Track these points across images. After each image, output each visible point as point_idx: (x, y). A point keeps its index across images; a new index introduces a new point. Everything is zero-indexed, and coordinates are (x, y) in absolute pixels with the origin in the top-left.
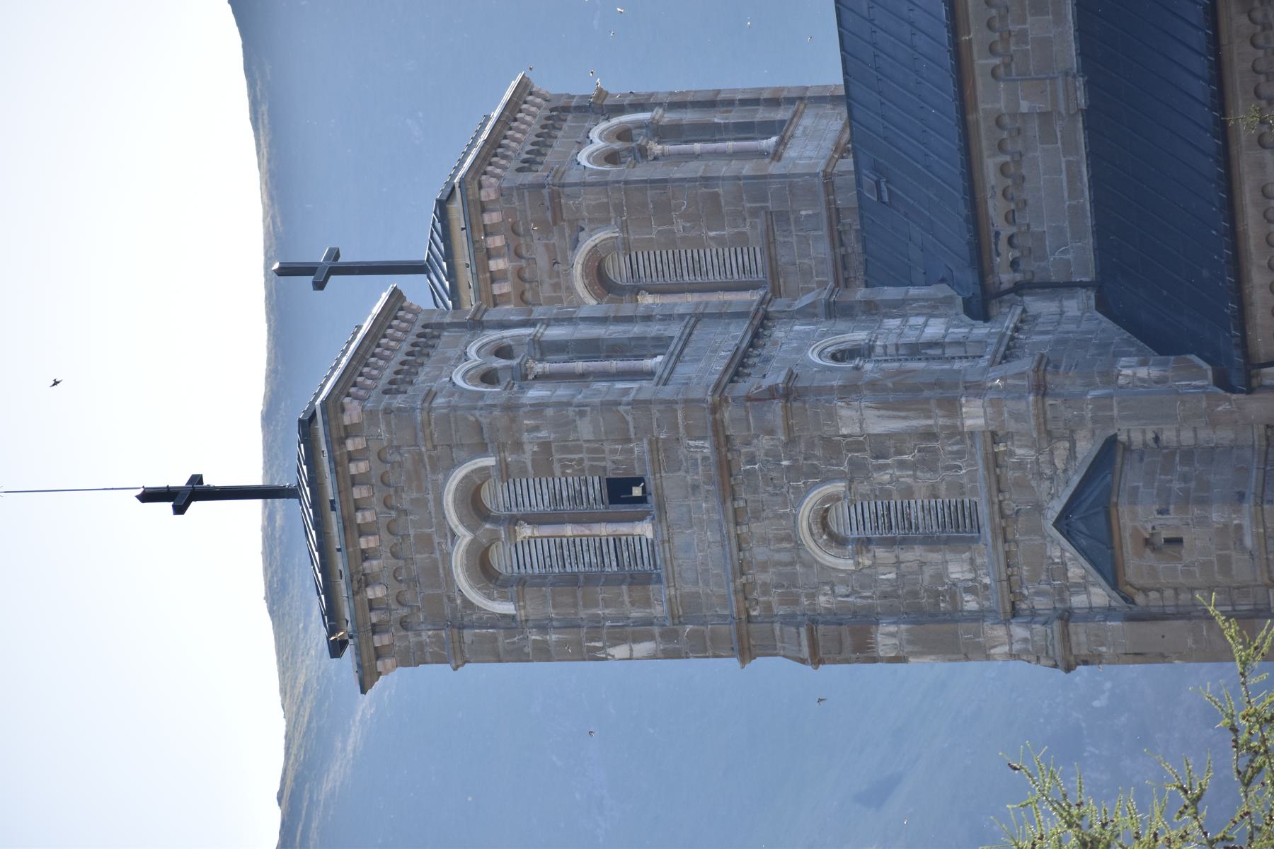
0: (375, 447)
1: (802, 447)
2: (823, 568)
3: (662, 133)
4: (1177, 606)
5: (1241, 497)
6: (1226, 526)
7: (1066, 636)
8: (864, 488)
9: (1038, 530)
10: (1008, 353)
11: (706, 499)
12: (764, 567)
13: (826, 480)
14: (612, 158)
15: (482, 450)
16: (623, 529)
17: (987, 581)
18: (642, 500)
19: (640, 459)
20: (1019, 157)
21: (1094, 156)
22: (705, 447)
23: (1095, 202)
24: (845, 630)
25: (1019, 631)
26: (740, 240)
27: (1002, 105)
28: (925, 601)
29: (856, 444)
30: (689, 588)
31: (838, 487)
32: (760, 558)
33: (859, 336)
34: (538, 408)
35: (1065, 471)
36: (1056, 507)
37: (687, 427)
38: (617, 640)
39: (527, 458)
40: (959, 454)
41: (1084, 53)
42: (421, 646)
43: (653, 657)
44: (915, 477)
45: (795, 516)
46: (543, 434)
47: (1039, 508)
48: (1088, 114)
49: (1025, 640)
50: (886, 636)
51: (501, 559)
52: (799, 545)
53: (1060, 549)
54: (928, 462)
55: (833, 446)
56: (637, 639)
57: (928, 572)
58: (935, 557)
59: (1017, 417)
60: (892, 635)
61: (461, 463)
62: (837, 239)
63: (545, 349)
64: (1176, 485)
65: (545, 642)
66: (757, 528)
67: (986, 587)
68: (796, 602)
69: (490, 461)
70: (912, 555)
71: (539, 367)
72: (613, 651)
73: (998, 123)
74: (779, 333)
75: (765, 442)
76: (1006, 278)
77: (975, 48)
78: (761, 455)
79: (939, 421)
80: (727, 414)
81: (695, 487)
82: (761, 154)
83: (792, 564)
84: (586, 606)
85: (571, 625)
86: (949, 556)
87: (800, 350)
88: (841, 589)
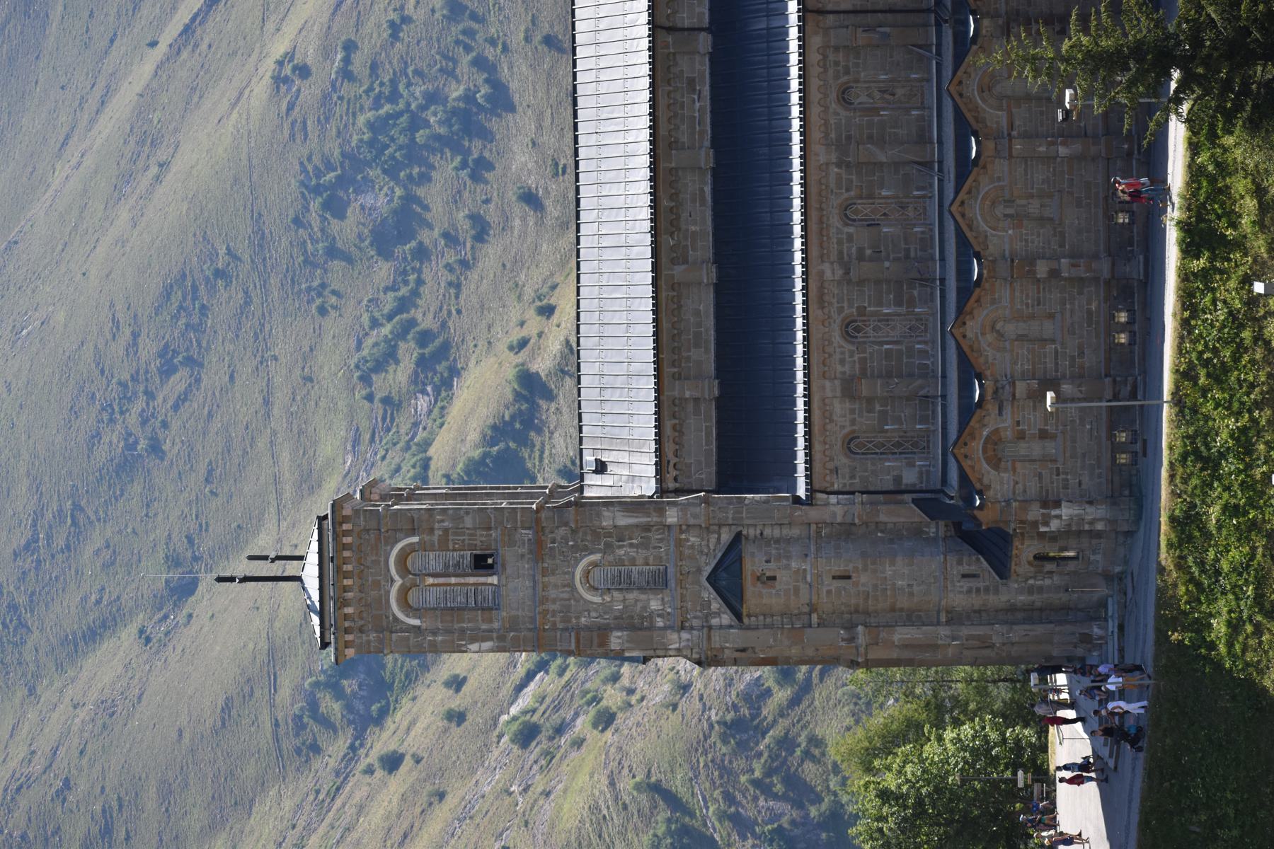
1: (581, 534)
2: (586, 601)
6: (799, 569)
7: (709, 638)
8: (611, 558)
11: (528, 563)
12: (554, 601)
15: (413, 532)
17: (669, 610)
18: (491, 567)
19: (496, 540)
21: (720, 422)
23: (719, 448)
24: (595, 634)
27: (676, 393)
30: (513, 613)
31: (596, 557)
32: (554, 596)
35: (714, 550)
37: (522, 522)
38: (473, 640)
39: (436, 538)
40: (661, 540)
42: (369, 642)
43: (492, 650)
44: (637, 552)
45: (574, 573)
46: (446, 524)
47: (699, 570)
48: (718, 400)
49: (688, 640)
50: (616, 640)
52: (574, 588)
53: (709, 593)
54: (645, 545)
56: (484, 640)
57: (639, 605)
58: (643, 597)
59: (695, 516)
60: (619, 637)
61: (400, 541)
64: (774, 552)
65: (435, 641)
66: (552, 579)
67: (669, 614)
68: (569, 621)
69: (415, 539)
70: (631, 596)
72: (470, 646)
77: (665, 363)
78: (558, 538)
79: (654, 519)
80: (543, 515)
81: (523, 556)
83: (569, 600)
84: (459, 622)
85: (448, 631)
86: (651, 597)
88: (594, 614)
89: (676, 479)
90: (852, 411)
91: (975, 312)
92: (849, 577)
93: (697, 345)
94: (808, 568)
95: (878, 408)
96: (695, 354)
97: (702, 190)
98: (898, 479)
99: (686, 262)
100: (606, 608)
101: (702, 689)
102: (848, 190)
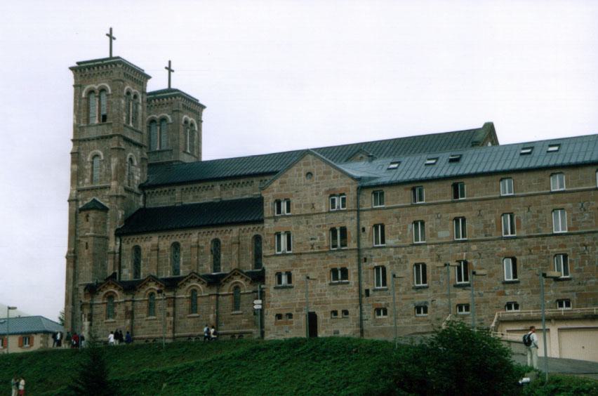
4: (174, 338)
5: (95, 233)
14: (186, 122)
15: (112, 91)
16: (97, 118)
20: (168, 194)
22: (111, 133)
25: (74, 192)
26: (168, 144)
29: (110, 162)
31: (102, 158)
33: (135, 163)
34: (120, 102)
36: (98, 199)
47: (97, 195)
51: (92, 96)
53: (90, 200)
63: (137, 104)
64: (98, 221)
70: (90, 172)
71: (131, 103)
74: (137, 149)
76: (147, 191)
82: (186, 149)
87: (132, 152)
89: (149, 193)
93: (194, 197)
94: (317, 241)
96: (191, 197)
97: (246, 194)
98: (124, 267)
99: (221, 190)
102: (224, 241)
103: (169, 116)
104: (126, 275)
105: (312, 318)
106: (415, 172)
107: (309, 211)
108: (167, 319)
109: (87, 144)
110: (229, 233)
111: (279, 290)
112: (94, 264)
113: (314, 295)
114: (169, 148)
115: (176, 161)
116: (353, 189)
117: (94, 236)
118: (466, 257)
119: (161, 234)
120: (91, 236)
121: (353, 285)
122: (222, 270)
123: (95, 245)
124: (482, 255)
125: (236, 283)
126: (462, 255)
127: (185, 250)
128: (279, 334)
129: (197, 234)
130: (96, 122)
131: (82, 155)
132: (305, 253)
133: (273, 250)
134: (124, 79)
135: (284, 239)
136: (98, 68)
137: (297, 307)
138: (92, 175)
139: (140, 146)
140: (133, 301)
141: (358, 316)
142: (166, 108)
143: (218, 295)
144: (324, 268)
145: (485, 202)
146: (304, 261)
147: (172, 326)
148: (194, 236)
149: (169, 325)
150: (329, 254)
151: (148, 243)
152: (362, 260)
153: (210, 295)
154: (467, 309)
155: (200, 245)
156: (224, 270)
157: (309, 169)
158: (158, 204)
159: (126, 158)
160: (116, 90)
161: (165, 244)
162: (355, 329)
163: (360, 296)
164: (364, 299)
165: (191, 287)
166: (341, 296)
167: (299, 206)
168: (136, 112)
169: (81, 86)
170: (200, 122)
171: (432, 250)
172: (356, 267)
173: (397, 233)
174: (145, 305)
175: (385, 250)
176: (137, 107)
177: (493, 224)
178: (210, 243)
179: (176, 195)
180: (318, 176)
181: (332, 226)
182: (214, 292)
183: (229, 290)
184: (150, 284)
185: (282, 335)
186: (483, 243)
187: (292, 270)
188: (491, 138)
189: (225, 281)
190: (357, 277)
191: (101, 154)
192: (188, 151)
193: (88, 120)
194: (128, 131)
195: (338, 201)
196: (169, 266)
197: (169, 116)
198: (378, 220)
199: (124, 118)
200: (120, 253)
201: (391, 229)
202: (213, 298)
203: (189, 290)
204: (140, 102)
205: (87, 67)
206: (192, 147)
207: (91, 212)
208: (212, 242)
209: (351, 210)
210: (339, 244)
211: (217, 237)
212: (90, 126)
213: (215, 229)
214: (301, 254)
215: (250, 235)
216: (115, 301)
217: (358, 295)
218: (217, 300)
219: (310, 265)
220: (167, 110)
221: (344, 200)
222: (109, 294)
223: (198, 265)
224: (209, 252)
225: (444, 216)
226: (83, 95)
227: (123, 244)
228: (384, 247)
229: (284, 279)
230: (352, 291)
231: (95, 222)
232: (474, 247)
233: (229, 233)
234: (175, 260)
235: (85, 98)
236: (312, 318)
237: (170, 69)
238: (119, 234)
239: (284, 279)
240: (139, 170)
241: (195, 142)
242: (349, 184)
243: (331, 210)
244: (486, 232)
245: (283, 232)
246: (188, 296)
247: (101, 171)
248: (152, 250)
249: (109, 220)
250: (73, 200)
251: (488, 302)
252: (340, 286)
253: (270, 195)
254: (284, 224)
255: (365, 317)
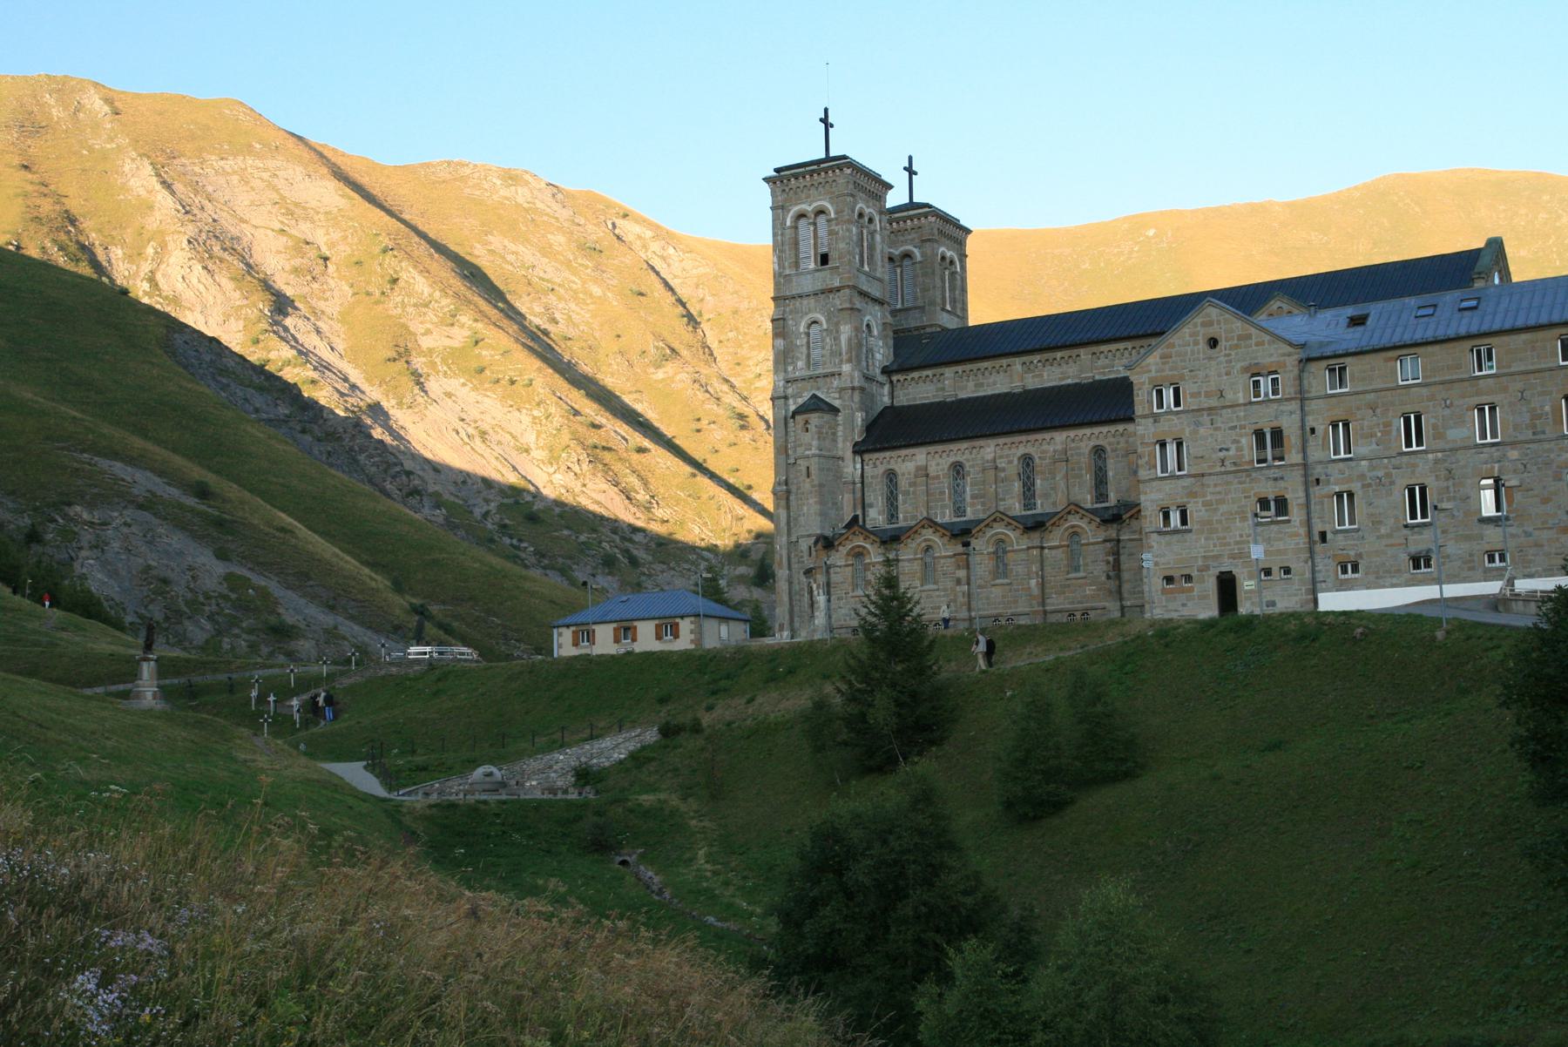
0: (837, 179)
3: (953, 274)
5: (821, 450)
8: (825, 334)
9: (812, 388)
10: (868, 378)
12: (801, 303)
13: (827, 321)
14: (943, 258)
15: (836, 213)
16: (813, 259)
22: (837, 284)
25: (781, 384)
28: (791, 355)
31: (825, 326)
33: (875, 332)
34: (849, 230)
36: (819, 394)
41: (962, 400)
47: (818, 389)
50: (780, 342)
51: (803, 222)
52: (807, 314)
53: (806, 396)
55: (837, 324)
58: (804, 357)
62: (917, 329)
63: (872, 233)
69: (833, 216)
70: (804, 350)
71: (865, 231)
73: (942, 374)
74: (877, 308)
75: (838, 303)
79: (845, 357)
82: (944, 303)
87: (871, 314)
89: (898, 381)
90: (909, 474)
91: (938, 534)
92: (808, 477)
93: (976, 385)
95: (912, 489)
96: (971, 384)
97: (1069, 377)
98: (871, 506)
100: (798, 336)
101: (269, 174)
102: (1040, 458)
103: (916, 251)
104: (875, 519)
105: (1227, 587)
106: (1389, 331)
107: (1213, 402)
108: (958, 588)
109: (798, 303)
110: (1049, 444)
111: (1168, 537)
112: (822, 503)
113: (1229, 544)
114: (920, 303)
115: (932, 326)
116: (1291, 362)
117: (819, 456)
118: (1500, 471)
119: (932, 449)
120: (814, 456)
121: (1298, 523)
122: (1039, 505)
123: (821, 470)
124: (1528, 466)
125: (1073, 527)
126: (1493, 468)
127: (973, 474)
128: (1170, 608)
129: (992, 448)
130: (812, 266)
131: (790, 322)
132: (1210, 474)
133: (1153, 471)
134: (855, 192)
135: (1171, 450)
136: (811, 176)
137: (1200, 563)
138: (808, 355)
139: (881, 303)
140: (1042, 548)
141: (1308, 575)
142: (910, 237)
143: (1042, 548)
144: (1245, 497)
145: (1532, 375)
146: (1209, 486)
147: (966, 599)
148: (989, 450)
149: (961, 599)
150: (1254, 475)
151: (909, 462)
152: (1311, 481)
153: (1029, 548)
154: (1355, 569)
155: (999, 466)
156: (1041, 506)
157: (1213, 331)
158: (915, 399)
159: (862, 324)
160: (842, 211)
161: (938, 464)
162: (1304, 597)
163: (1311, 543)
164: (1319, 547)
165: (993, 536)
166: (1276, 543)
167: (1195, 395)
168: (872, 248)
169: (783, 208)
170: (963, 256)
171: (1436, 461)
172: (1301, 494)
173: (1372, 435)
174: (917, 566)
175: (1353, 464)
176: (873, 238)
177: (1547, 414)
178: (1016, 462)
179: (946, 382)
180: (1228, 344)
181: (1258, 427)
182: (1037, 543)
183: (1061, 540)
184: (924, 531)
185: (1176, 611)
186: (1530, 446)
187: (1189, 502)
188: (1497, 263)
189: (1053, 524)
190: (1304, 512)
191: (822, 319)
192: (948, 308)
193: (797, 264)
194: (863, 278)
195: (1265, 384)
196: (947, 502)
197: (916, 251)
198: (1339, 413)
199: (857, 257)
200: (862, 483)
201: (1362, 429)
202: (1035, 552)
203: (992, 541)
204: (878, 229)
205: (793, 175)
206: (954, 301)
207: (813, 415)
208: (1019, 459)
209: (1292, 399)
210: (1270, 457)
211: (1027, 451)
212: (802, 274)
213: (1023, 438)
214: (1203, 475)
215: (1086, 447)
216: (868, 561)
217: (1307, 540)
218: (1041, 555)
219: (1219, 493)
220: (913, 240)
221: (1275, 381)
222: (857, 550)
223: (997, 499)
224: (1016, 478)
225: (1456, 402)
226: (788, 223)
227: (866, 467)
228: (1350, 459)
229: (1175, 518)
230: (1298, 535)
231: (820, 433)
232: (1514, 454)
233: (1049, 444)
234: (957, 492)
235: (791, 227)
236: (1227, 587)
237: (825, 121)
238: (860, 450)
239: (1175, 518)
240: (881, 343)
241: (957, 292)
242: (1284, 355)
243: (1253, 400)
244: (1534, 426)
245: (1168, 440)
246: (991, 550)
247: (823, 348)
248: (916, 476)
249: (840, 428)
250: (779, 398)
251: (1542, 546)
252: (1274, 528)
253: (1145, 378)
254: (1171, 426)
255: (1319, 577)
